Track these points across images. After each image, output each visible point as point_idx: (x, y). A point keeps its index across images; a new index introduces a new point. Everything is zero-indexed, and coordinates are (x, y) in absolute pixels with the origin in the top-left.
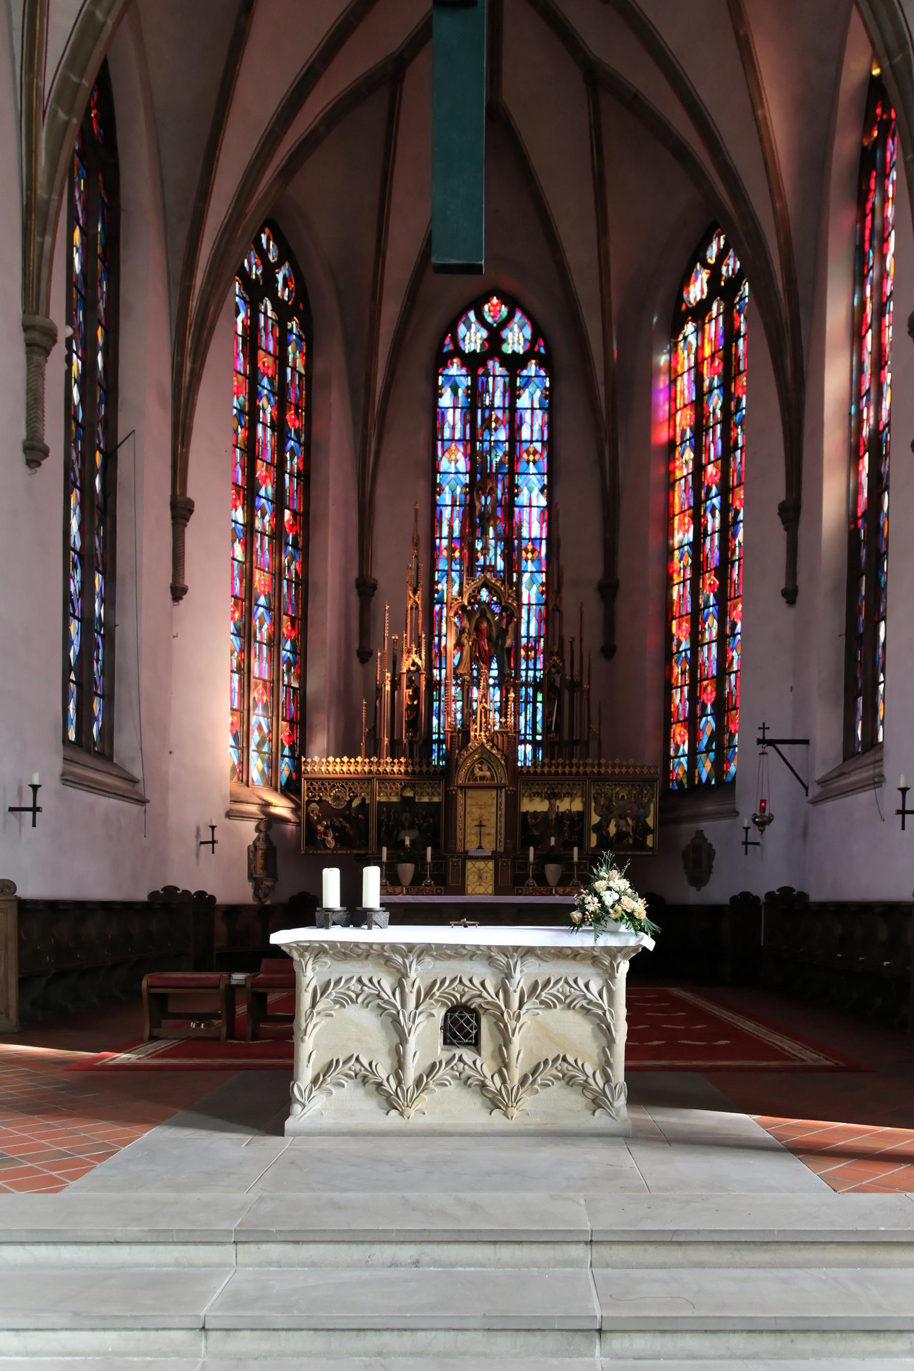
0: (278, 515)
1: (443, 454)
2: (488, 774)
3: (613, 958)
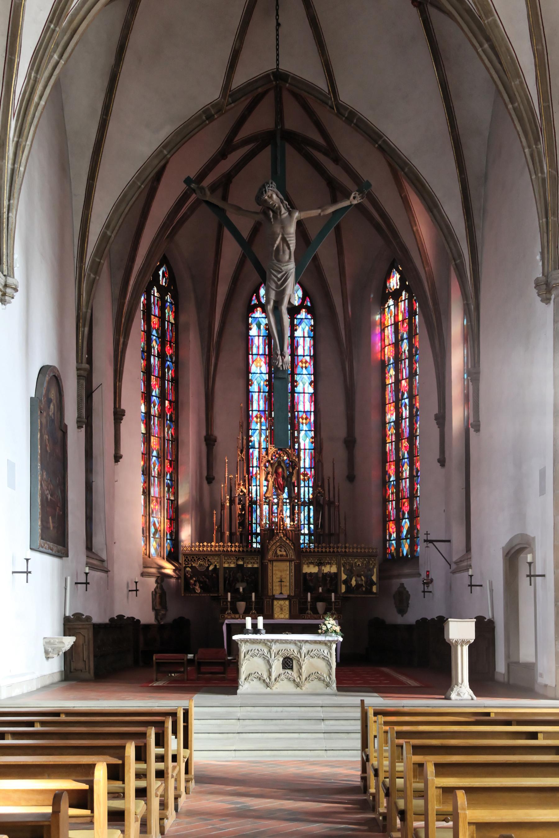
0: (162, 404)
1: (253, 362)
2: (284, 553)
3: (331, 643)
